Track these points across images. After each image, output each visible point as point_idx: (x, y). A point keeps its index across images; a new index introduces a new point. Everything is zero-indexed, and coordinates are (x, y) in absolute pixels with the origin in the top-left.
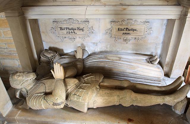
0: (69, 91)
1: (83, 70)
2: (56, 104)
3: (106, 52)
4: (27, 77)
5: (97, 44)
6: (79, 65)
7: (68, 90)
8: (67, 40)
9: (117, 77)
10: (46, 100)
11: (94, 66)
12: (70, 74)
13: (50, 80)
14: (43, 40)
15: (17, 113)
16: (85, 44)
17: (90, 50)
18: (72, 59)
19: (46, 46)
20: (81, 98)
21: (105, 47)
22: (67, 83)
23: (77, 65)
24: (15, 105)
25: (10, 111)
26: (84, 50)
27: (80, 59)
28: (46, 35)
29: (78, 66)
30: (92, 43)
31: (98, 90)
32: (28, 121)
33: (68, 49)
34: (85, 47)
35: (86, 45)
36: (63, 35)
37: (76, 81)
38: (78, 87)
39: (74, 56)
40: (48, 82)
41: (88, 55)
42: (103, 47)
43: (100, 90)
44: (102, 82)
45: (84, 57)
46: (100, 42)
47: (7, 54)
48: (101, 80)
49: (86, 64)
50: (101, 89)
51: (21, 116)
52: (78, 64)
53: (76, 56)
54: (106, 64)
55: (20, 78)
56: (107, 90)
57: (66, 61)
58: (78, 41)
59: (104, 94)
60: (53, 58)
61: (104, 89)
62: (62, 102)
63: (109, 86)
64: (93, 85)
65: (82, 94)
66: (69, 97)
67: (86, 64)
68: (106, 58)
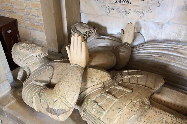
0: (88, 91)
1: (128, 63)
2: (52, 111)
3: (178, 42)
4: (32, 52)
5: (163, 25)
6: (123, 53)
7: (86, 89)
8: (116, 13)
9: (183, 87)
10: (40, 97)
11: (148, 60)
12: (102, 62)
13: (64, 65)
14: (81, 10)
15: (9, 102)
16: (142, 23)
17: (148, 34)
18: (116, 42)
19: (84, 19)
20: (104, 113)
21: (176, 33)
22: (88, 76)
23: (121, 51)
24: (14, 90)
25: (4, 96)
26: (137, 33)
27: (128, 43)
28: (86, 3)
29: (121, 53)
30: (154, 23)
31: (146, 107)
32: (18, 120)
33: (114, 30)
34: (141, 28)
35: (143, 26)
36: (109, 4)
37: (106, 77)
38: (107, 90)
39: (120, 40)
40: (59, 66)
41: (142, 42)
42: (173, 33)
43: (149, 108)
44: (159, 92)
45: (135, 43)
46: (168, 22)
47: (37, 24)
48: (157, 88)
49: (136, 53)
50: (154, 108)
51: (11, 109)
52: (121, 50)
53: (122, 39)
54: (172, 61)
55: (24, 51)
56: (166, 113)
57: (104, 43)
58: (133, 17)
59: (158, 120)
60: (86, 36)
61: (160, 109)
62: (62, 110)
63: (172, 104)
64: (137, 94)
65: (107, 106)
66: (84, 103)
67: (136, 53)
68: (175, 50)
